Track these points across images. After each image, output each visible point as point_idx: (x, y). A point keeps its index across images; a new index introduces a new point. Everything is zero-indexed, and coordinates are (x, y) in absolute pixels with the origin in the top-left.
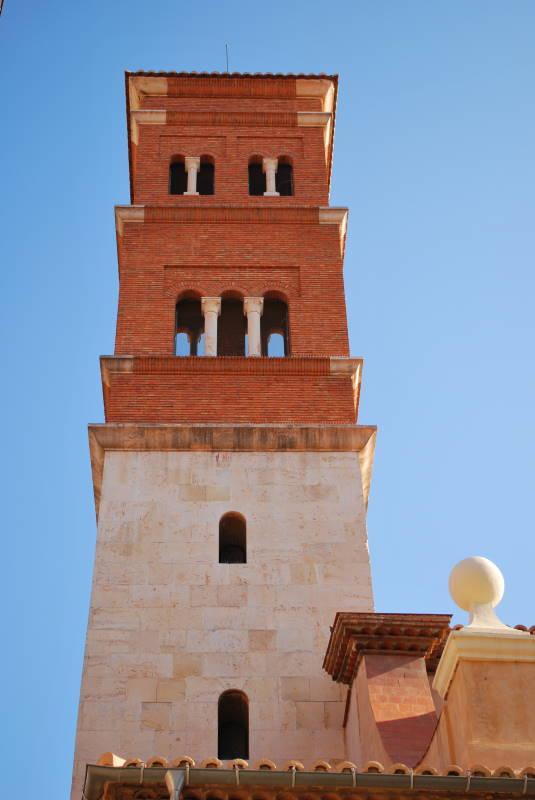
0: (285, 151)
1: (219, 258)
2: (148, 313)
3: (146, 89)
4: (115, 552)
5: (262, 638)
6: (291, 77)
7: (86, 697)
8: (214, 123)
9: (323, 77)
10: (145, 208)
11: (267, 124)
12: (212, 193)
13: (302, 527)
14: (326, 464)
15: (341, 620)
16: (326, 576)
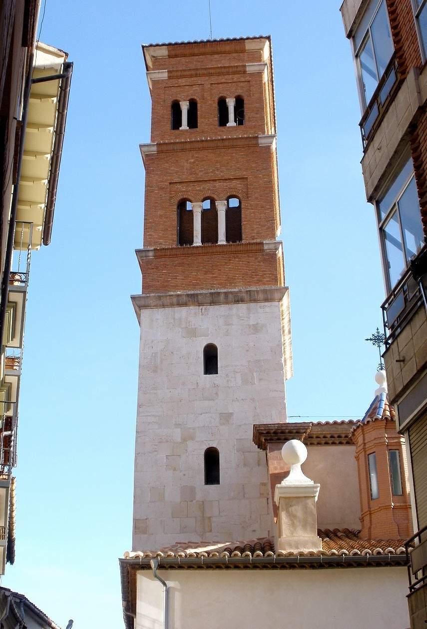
0: (239, 92)
1: (201, 175)
2: (161, 216)
3: (155, 55)
4: (149, 371)
5: (226, 417)
6: (242, 39)
7: (138, 454)
8: (196, 75)
9: (261, 37)
10: (157, 144)
11: (228, 74)
12: (196, 127)
13: (247, 351)
14: (260, 310)
15: (256, 428)
16: (260, 380)
